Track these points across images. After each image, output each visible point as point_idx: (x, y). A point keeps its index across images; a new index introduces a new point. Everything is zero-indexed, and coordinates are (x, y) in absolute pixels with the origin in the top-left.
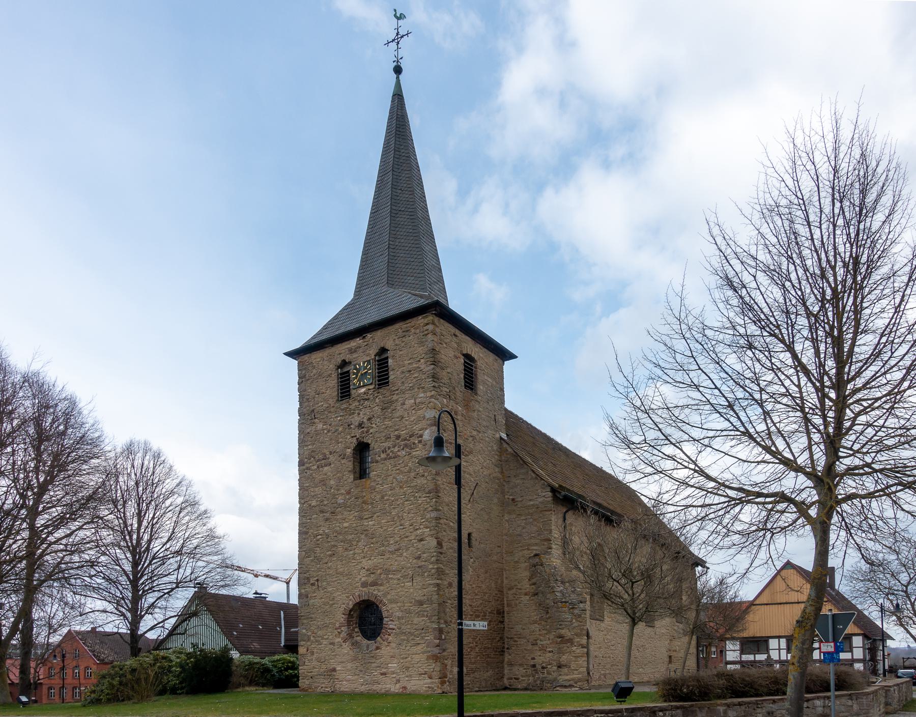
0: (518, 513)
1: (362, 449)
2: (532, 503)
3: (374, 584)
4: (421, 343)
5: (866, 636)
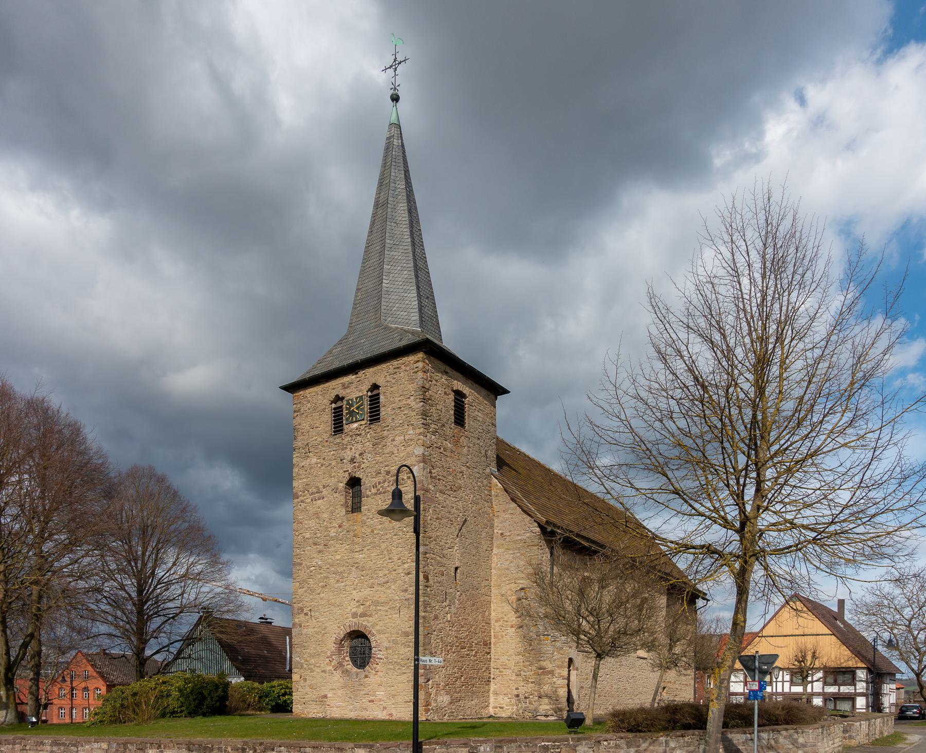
1: (354, 482)
3: (364, 615)
4: (411, 380)
5: (870, 671)
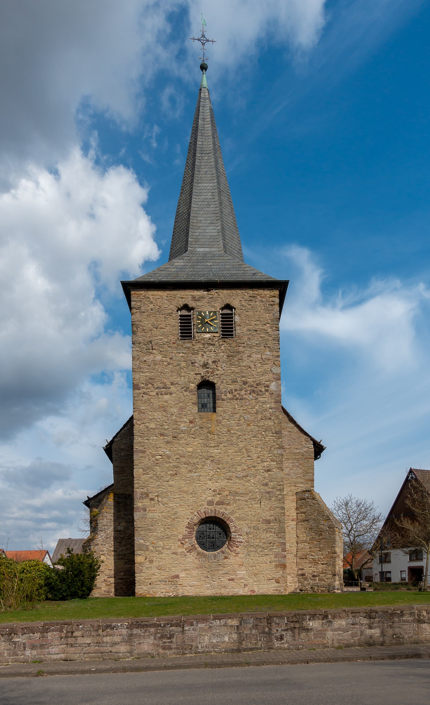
1: (206, 385)
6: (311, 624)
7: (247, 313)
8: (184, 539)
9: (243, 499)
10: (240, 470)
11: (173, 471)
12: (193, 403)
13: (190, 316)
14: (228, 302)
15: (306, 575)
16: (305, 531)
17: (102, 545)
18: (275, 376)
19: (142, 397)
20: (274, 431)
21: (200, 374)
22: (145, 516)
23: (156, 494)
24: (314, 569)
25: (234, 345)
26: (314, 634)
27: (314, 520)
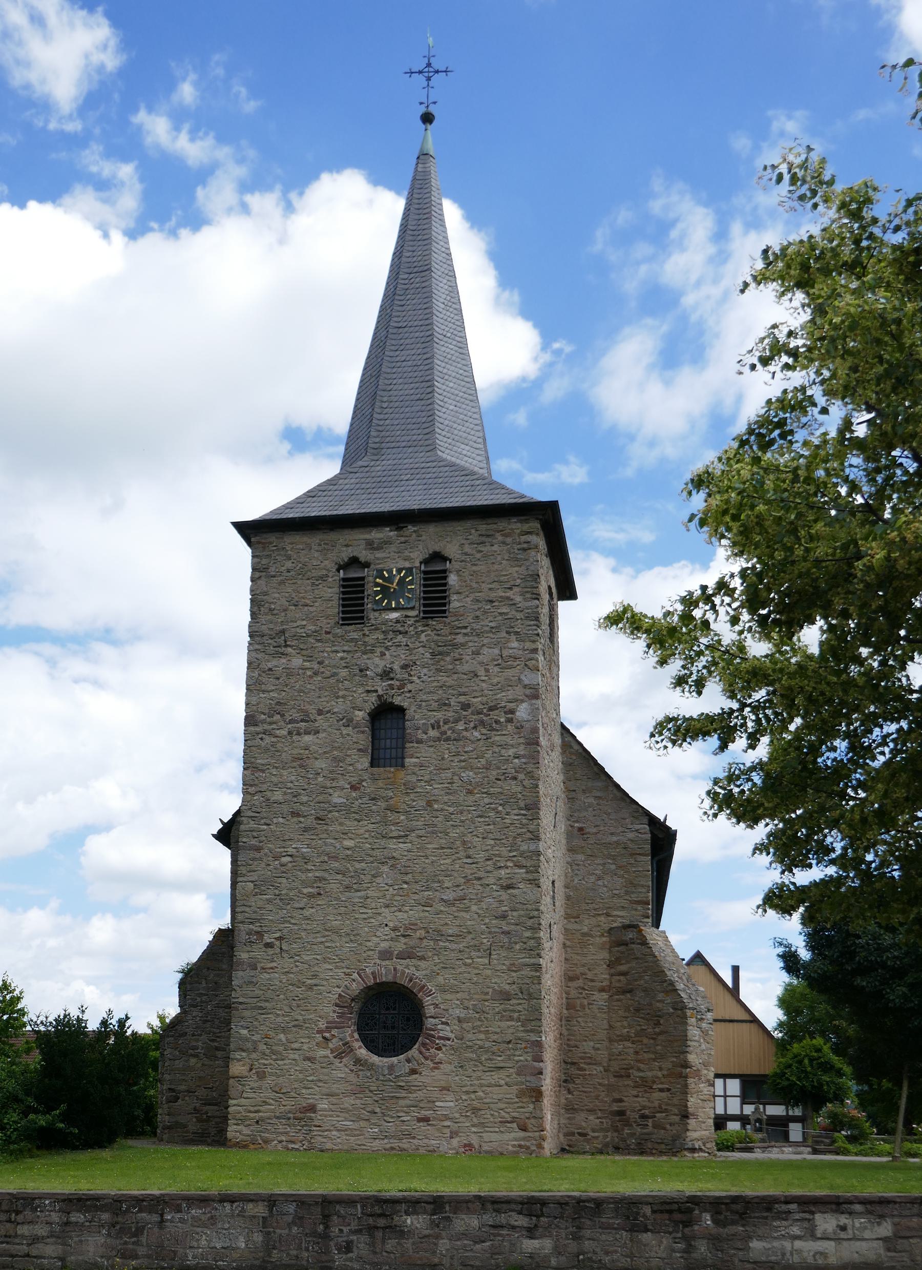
0: (589, 852)
1: (386, 715)
2: (615, 839)
6: (409, 1221)
7: (474, 568)
8: (328, 1029)
9: (454, 946)
10: (450, 885)
11: (313, 887)
12: (359, 750)
13: (363, 579)
14: (437, 549)
15: (628, 1113)
16: (627, 1014)
17: (193, 1035)
18: (528, 692)
19: (261, 739)
20: (522, 804)
21: (376, 691)
22: (254, 980)
23: (277, 935)
24: (642, 1101)
25: (446, 630)
26: (413, 1244)
27: (645, 990)
